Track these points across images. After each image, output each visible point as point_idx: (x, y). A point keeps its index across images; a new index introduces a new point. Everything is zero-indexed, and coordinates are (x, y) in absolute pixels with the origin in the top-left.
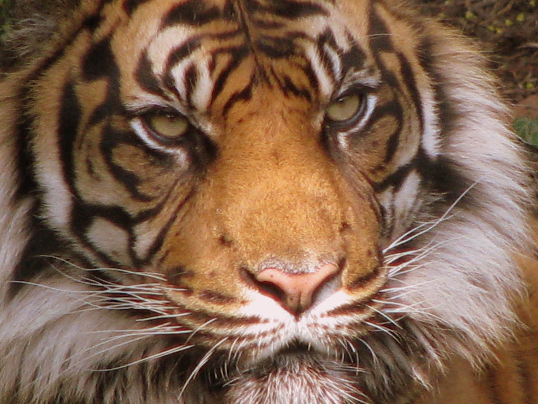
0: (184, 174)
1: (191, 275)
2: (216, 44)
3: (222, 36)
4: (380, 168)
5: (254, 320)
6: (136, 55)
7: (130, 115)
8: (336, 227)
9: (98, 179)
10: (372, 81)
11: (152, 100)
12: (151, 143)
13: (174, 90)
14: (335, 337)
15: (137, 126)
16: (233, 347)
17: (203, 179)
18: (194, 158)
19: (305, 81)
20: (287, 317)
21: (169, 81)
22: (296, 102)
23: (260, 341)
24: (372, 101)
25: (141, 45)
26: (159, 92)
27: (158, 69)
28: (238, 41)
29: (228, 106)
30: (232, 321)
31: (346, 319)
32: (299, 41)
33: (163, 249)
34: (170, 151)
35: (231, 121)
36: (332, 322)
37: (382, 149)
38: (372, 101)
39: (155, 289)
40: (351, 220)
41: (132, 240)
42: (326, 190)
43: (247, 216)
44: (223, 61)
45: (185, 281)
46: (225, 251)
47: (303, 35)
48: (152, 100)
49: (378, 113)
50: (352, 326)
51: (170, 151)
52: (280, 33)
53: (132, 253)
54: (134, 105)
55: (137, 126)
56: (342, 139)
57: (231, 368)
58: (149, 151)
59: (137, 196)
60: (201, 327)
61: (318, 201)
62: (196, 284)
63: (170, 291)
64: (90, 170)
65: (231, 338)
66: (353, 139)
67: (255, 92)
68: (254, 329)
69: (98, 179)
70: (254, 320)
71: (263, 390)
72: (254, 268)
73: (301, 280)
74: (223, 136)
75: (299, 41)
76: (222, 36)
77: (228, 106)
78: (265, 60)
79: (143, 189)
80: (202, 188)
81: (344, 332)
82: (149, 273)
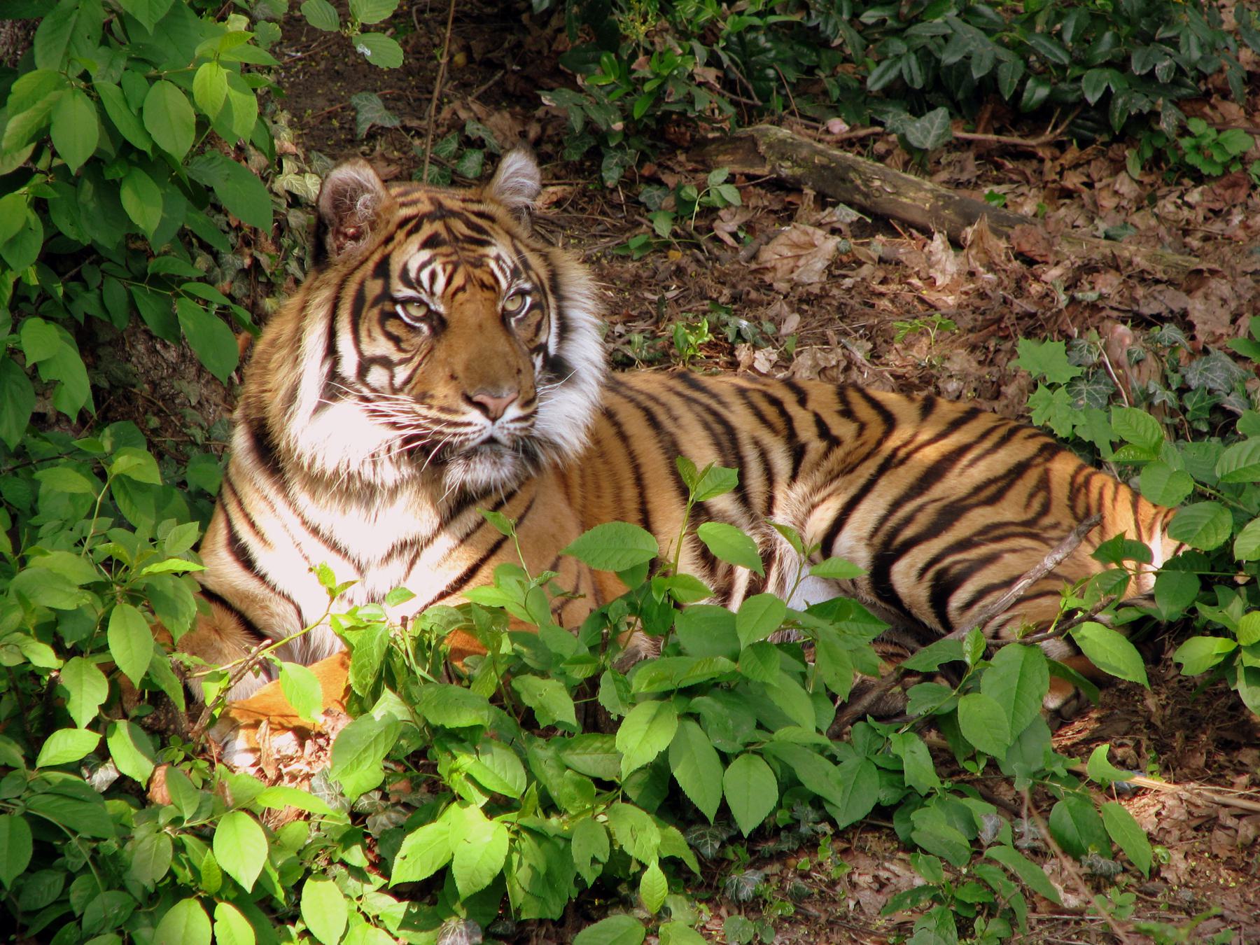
0: (426, 338)
1: (432, 397)
2: (444, 259)
3: (447, 255)
4: (532, 340)
5: (469, 424)
6: (401, 264)
7: (395, 301)
8: (515, 371)
9: (374, 340)
10: (527, 286)
11: (410, 293)
12: (407, 320)
13: (422, 287)
14: (513, 435)
15: (399, 309)
16: (456, 440)
17: (438, 341)
18: (432, 328)
19: (492, 281)
20: (488, 423)
21: (419, 282)
22: (488, 294)
23: (471, 437)
24: (529, 300)
25: (405, 258)
26: (415, 289)
27: (412, 274)
28: (454, 258)
29: (454, 294)
30: (456, 424)
31: (518, 425)
32: (486, 259)
33: (413, 382)
34: (417, 325)
35: (456, 303)
36: (512, 426)
37: (533, 328)
38: (529, 300)
39: (406, 407)
40: (522, 367)
41: (392, 377)
42: (507, 349)
43: (1152, 243)
44: (449, 268)
45: (428, 401)
46: (454, 383)
47: (487, 256)
48: (410, 293)
49: (532, 307)
50: (522, 429)
51: (417, 325)
52: (476, 255)
53: (391, 384)
54: (399, 295)
55: (399, 309)
56: (513, 321)
57: (452, 452)
58: (407, 325)
59: (400, 350)
60: (436, 428)
61: (505, 355)
62: (435, 403)
63: (418, 407)
64: (370, 336)
65: (455, 435)
66: (518, 321)
67: (468, 287)
68: (468, 429)
69: (374, 340)
70: (469, 424)
71: (468, 465)
72: (471, 394)
73: (497, 401)
74: (450, 314)
75: (486, 259)
76: (447, 255)
77: (454, 294)
78: (471, 269)
79: (404, 345)
80: (437, 346)
81: (518, 433)
82: (401, 396)
